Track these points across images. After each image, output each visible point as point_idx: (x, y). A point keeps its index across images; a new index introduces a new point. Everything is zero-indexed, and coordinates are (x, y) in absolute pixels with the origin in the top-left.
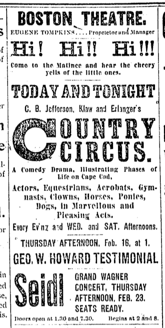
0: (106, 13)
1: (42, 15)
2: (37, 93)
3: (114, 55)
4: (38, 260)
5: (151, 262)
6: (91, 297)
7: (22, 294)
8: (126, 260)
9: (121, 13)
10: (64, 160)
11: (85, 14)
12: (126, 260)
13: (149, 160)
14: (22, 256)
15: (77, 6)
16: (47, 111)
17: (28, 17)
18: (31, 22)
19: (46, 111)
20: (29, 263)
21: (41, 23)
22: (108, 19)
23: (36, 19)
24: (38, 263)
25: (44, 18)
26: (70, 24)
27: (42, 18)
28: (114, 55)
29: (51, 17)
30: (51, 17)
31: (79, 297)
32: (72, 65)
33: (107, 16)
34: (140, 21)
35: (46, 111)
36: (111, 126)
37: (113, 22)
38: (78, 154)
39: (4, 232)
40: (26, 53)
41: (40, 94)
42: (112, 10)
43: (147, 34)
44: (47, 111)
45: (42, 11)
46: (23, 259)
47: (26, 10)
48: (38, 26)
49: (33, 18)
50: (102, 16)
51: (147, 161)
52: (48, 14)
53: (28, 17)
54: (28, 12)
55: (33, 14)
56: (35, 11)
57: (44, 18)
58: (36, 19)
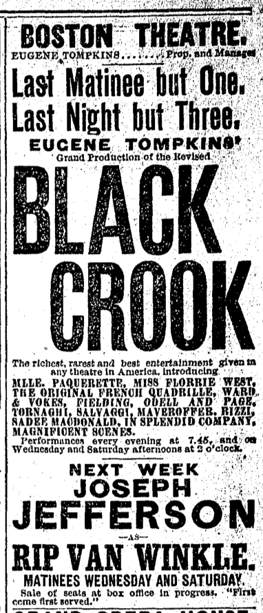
0: (177, 25)
1: (62, 32)
9: (202, 26)
11: (141, 27)
15: (132, 14)
17: (47, 39)
18: (43, 31)
21: (61, 44)
22: (180, 35)
23: (52, 37)
25: (66, 36)
26: (109, 44)
27: (62, 35)
29: (78, 33)
30: (78, 33)
32: (151, 440)
33: (179, 30)
34: (236, 38)
36: (81, 290)
37: (187, 40)
38: (14, 115)
40: (42, 578)
42: (189, 19)
43: (244, 57)
45: (64, 22)
47: (35, 23)
48: (41, 74)
49: (38, 38)
50: (170, 32)
51: (155, 498)
52: (72, 28)
53: (47, 39)
54: (53, 150)
55: (47, 28)
56: (51, 23)
57: (66, 36)
58: (52, 37)
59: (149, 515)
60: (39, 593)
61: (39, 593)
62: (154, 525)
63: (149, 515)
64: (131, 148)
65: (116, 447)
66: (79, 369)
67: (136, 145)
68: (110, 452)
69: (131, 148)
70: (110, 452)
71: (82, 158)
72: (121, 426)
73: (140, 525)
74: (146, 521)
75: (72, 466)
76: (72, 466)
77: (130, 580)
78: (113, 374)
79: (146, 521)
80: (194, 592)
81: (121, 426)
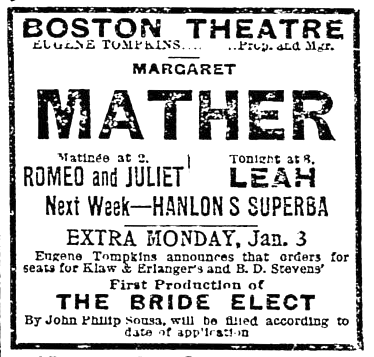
2: (205, 239)
3: (313, 297)
4: (92, 208)
5: (174, 214)
6: (291, 202)
7: (172, 92)
8: (54, 178)
10: (80, 168)
12: (54, 178)
13: (238, 245)
14: (288, 201)
16: (129, 185)
19: (127, 186)
20: (208, 214)
24: (92, 214)
28: (313, 297)
31: (62, 172)
35: (127, 186)
39: (345, 260)
41: (208, 242)
44: (129, 185)
46: (289, 206)
59: (313, 30)
60: (79, 257)
61: (79, 257)
62: (160, 308)
63: (313, 30)
64: (64, 306)
65: (124, 262)
66: (214, 264)
67: (70, 302)
68: (297, 324)
69: (64, 306)
70: (297, 324)
71: (226, 270)
72: (84, 260)
73: (299, 134)
74: (155, 305)
75: (136, 66)
76: (136, 66)
77: (258, 205)
78: (239, 288)
79: (155, 305)
80: (264, 158)
81: (84, 260)
